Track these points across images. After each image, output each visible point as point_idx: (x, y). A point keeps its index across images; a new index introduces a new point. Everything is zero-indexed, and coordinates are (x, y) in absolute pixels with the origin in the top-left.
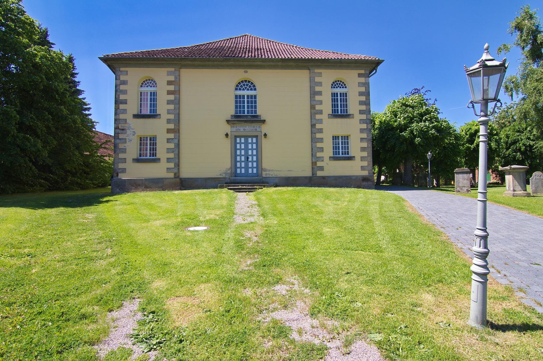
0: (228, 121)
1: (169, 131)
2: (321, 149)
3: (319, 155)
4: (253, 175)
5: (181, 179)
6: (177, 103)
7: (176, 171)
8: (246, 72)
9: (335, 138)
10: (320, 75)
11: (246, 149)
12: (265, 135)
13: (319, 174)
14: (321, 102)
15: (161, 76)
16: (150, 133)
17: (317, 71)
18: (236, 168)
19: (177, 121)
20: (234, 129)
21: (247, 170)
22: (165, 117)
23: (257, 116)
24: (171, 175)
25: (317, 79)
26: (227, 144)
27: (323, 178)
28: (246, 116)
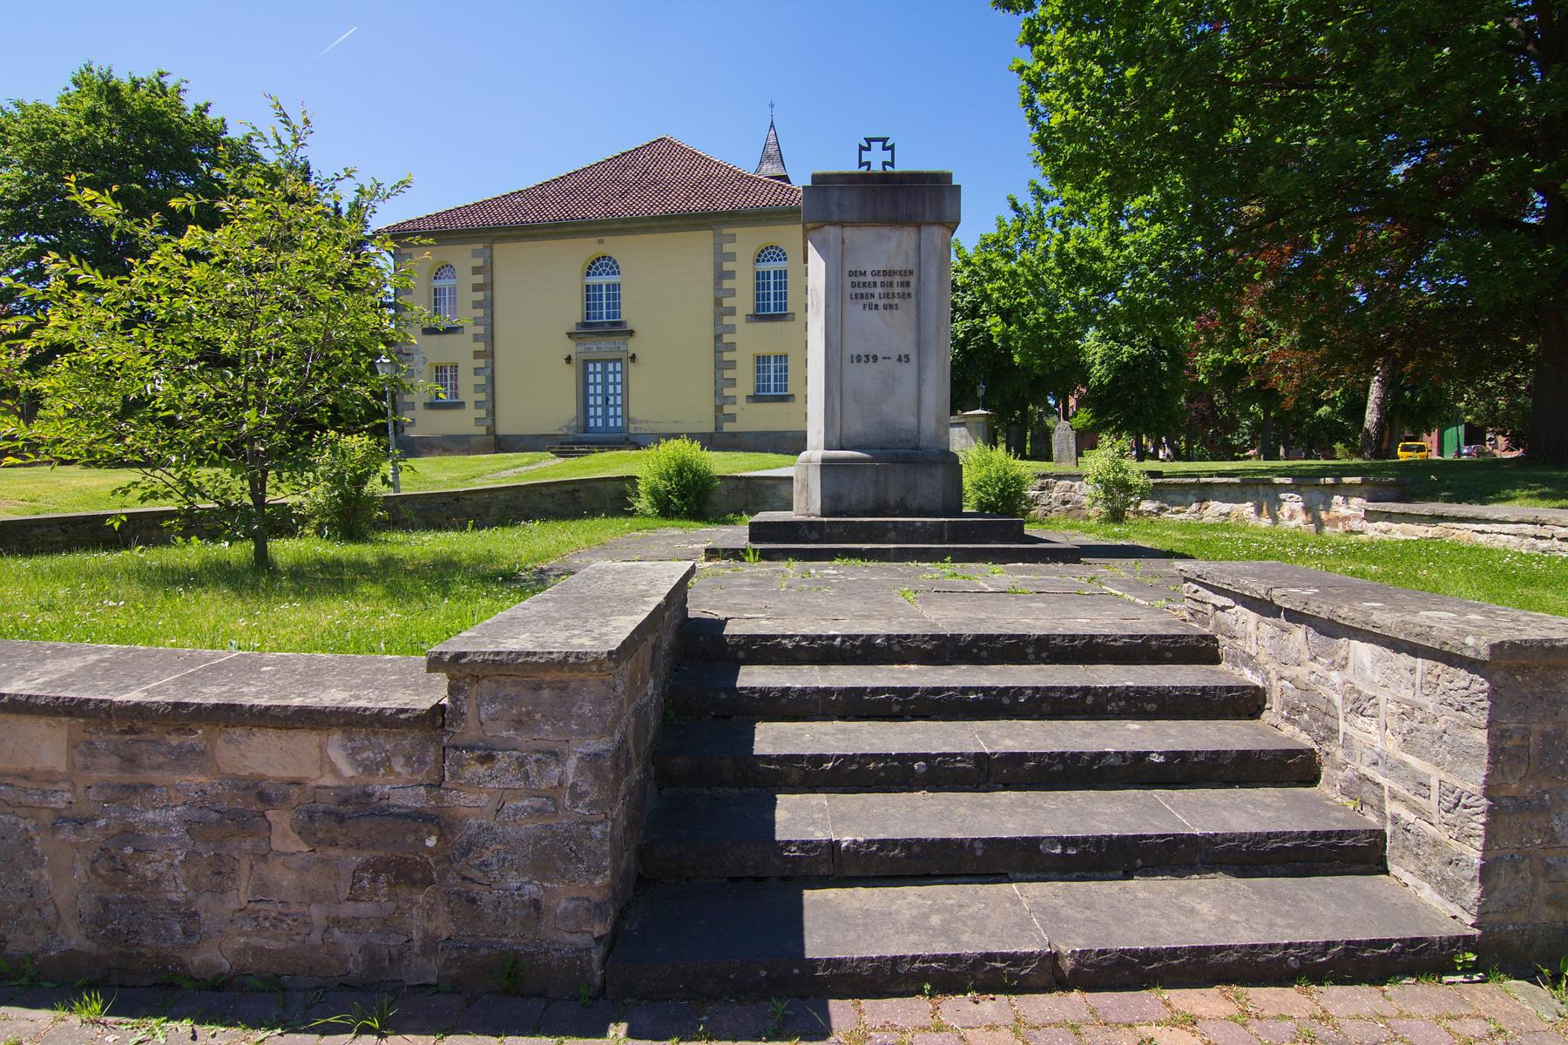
0: (570, 335)
1: (477, 355)
2: (732, 382)
3: (727, 392)
4: (616, 429)
5: (496, 437)
6: (488, 305)
7: (489, 422)
8: (601, 242)
9: (761, 360)
10: (733, 238)
11: (605, 384)
12: (633, 357)
13: (728, 427)
14: (732, 293)
15: (463, 257)
16: (446, 359)
17: (726, 231)
18: (586, 417)
19: (490, 337)
20: (581, 349)
21: (606, 422)
22: (471, 329)
23: (619, 324)
24: (482, 430)
25: (727, 248)
26: (570, 375)
27: (734, 435)
28: (602, 325)
